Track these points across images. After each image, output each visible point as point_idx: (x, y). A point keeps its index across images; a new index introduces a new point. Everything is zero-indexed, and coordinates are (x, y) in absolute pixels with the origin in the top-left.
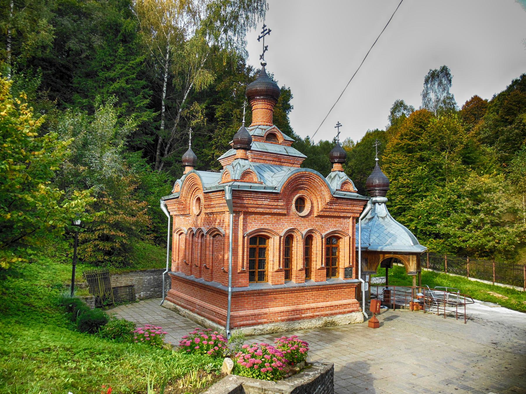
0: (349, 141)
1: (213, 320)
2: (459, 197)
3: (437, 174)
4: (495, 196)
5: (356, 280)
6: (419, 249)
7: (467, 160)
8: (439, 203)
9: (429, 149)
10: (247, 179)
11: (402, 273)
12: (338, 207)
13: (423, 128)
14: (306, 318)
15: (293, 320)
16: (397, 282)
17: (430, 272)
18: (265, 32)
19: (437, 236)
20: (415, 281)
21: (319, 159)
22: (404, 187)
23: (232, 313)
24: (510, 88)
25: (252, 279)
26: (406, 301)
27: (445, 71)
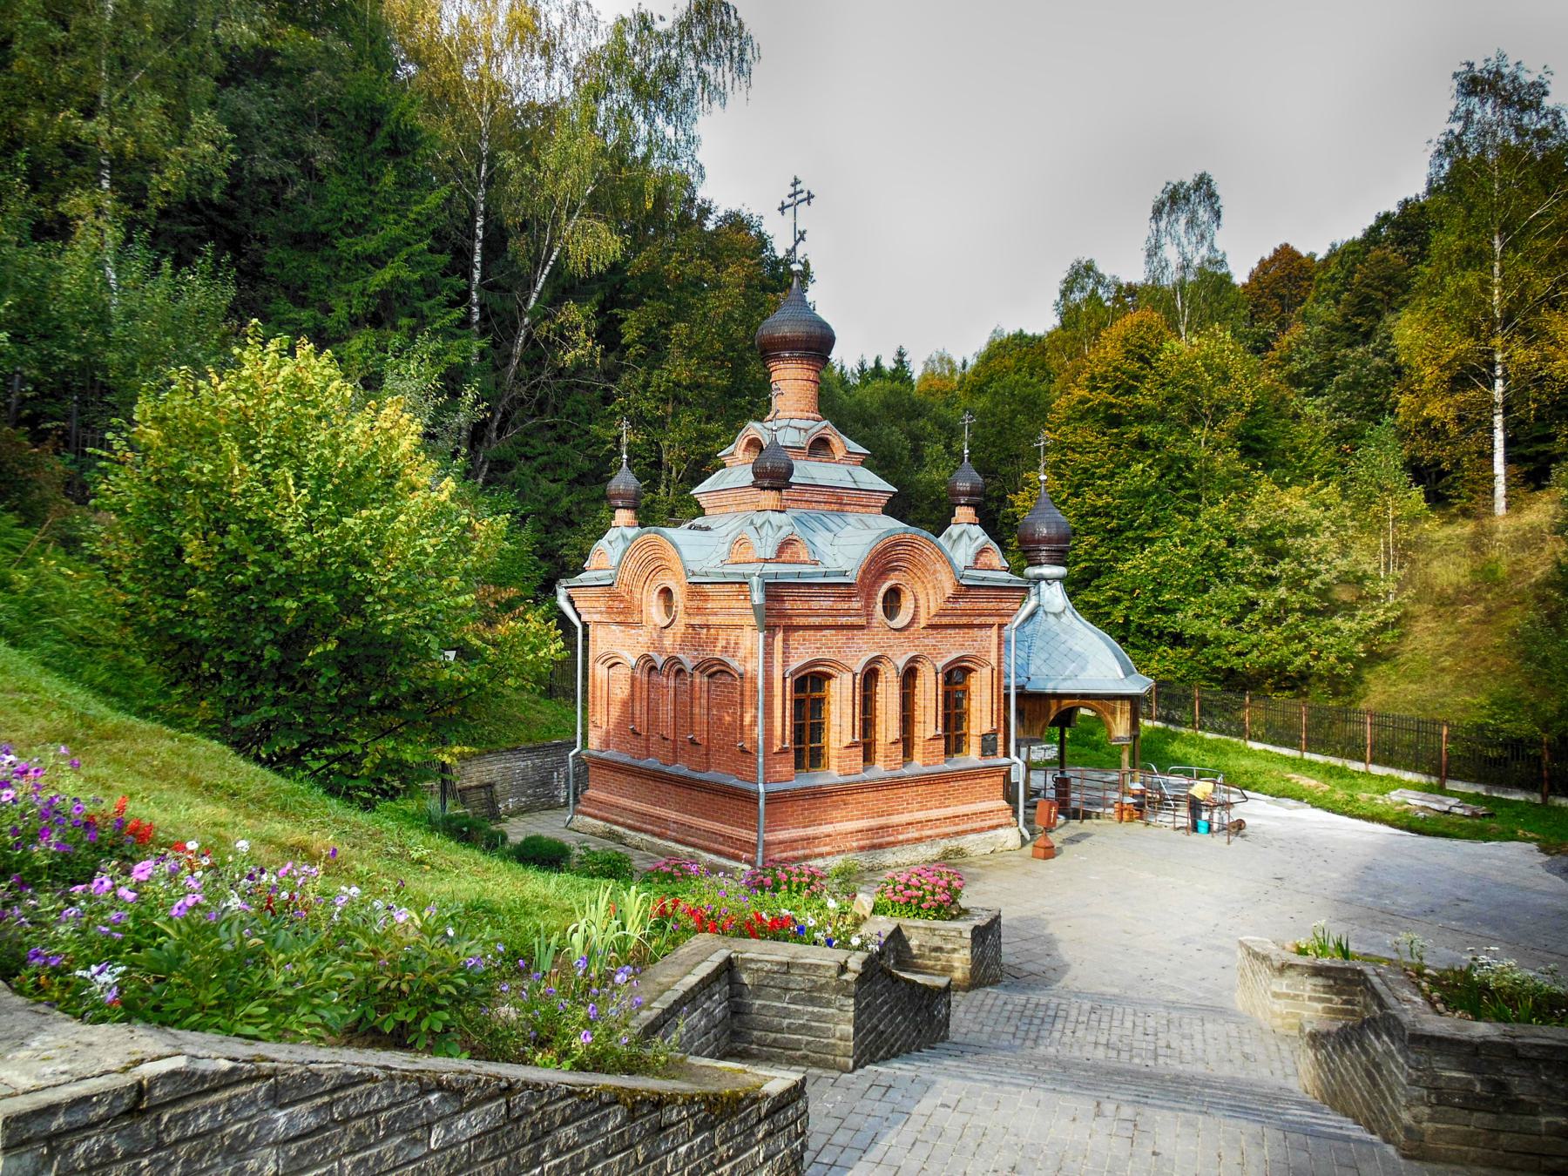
0: (941, 359)
1: (719, 853)
2: (1231, 542)
3: (1179, 484)
4: (1313, 544)
5: (1005, 761)
6: (1138, 685)
7: (1253, 444)
8: (1183, 558)
9: (1162, 419)
10: (786, 556)
11: (1093, 734)
12: (969, 606)
13: (1147, 362)
14: (907, 841)
15: (874, 847)
16: (1080, 756)
17: (1157, 730)
18: (799, 197)
19: (1177, 639)
20: (1125, 757)
21: (879, 437)
22: (1099, 515)
23: (770, 837)
24: (1372, 235)
25: (799, 765)
26: (1103, 803)
27: (1203, 182)
